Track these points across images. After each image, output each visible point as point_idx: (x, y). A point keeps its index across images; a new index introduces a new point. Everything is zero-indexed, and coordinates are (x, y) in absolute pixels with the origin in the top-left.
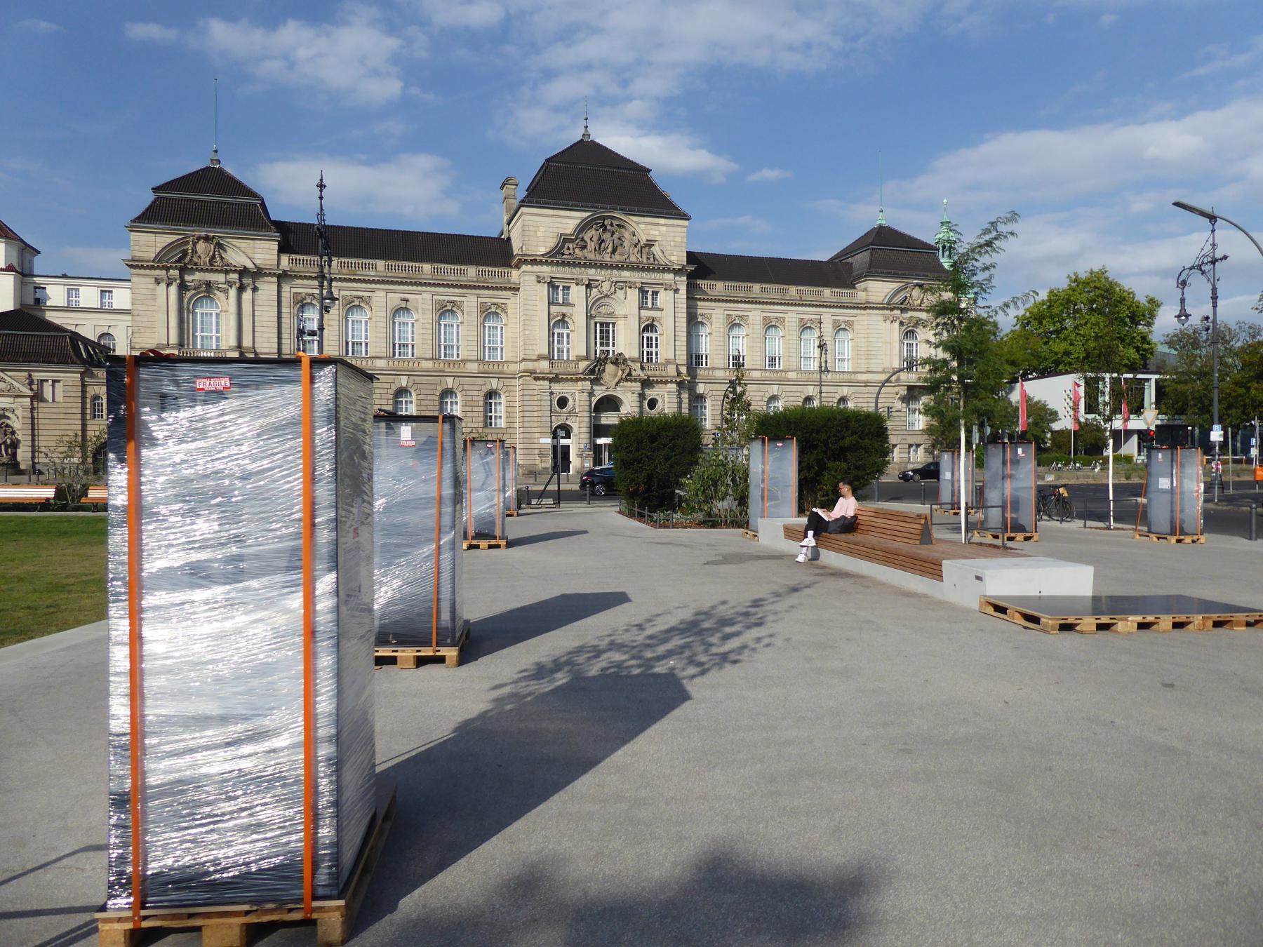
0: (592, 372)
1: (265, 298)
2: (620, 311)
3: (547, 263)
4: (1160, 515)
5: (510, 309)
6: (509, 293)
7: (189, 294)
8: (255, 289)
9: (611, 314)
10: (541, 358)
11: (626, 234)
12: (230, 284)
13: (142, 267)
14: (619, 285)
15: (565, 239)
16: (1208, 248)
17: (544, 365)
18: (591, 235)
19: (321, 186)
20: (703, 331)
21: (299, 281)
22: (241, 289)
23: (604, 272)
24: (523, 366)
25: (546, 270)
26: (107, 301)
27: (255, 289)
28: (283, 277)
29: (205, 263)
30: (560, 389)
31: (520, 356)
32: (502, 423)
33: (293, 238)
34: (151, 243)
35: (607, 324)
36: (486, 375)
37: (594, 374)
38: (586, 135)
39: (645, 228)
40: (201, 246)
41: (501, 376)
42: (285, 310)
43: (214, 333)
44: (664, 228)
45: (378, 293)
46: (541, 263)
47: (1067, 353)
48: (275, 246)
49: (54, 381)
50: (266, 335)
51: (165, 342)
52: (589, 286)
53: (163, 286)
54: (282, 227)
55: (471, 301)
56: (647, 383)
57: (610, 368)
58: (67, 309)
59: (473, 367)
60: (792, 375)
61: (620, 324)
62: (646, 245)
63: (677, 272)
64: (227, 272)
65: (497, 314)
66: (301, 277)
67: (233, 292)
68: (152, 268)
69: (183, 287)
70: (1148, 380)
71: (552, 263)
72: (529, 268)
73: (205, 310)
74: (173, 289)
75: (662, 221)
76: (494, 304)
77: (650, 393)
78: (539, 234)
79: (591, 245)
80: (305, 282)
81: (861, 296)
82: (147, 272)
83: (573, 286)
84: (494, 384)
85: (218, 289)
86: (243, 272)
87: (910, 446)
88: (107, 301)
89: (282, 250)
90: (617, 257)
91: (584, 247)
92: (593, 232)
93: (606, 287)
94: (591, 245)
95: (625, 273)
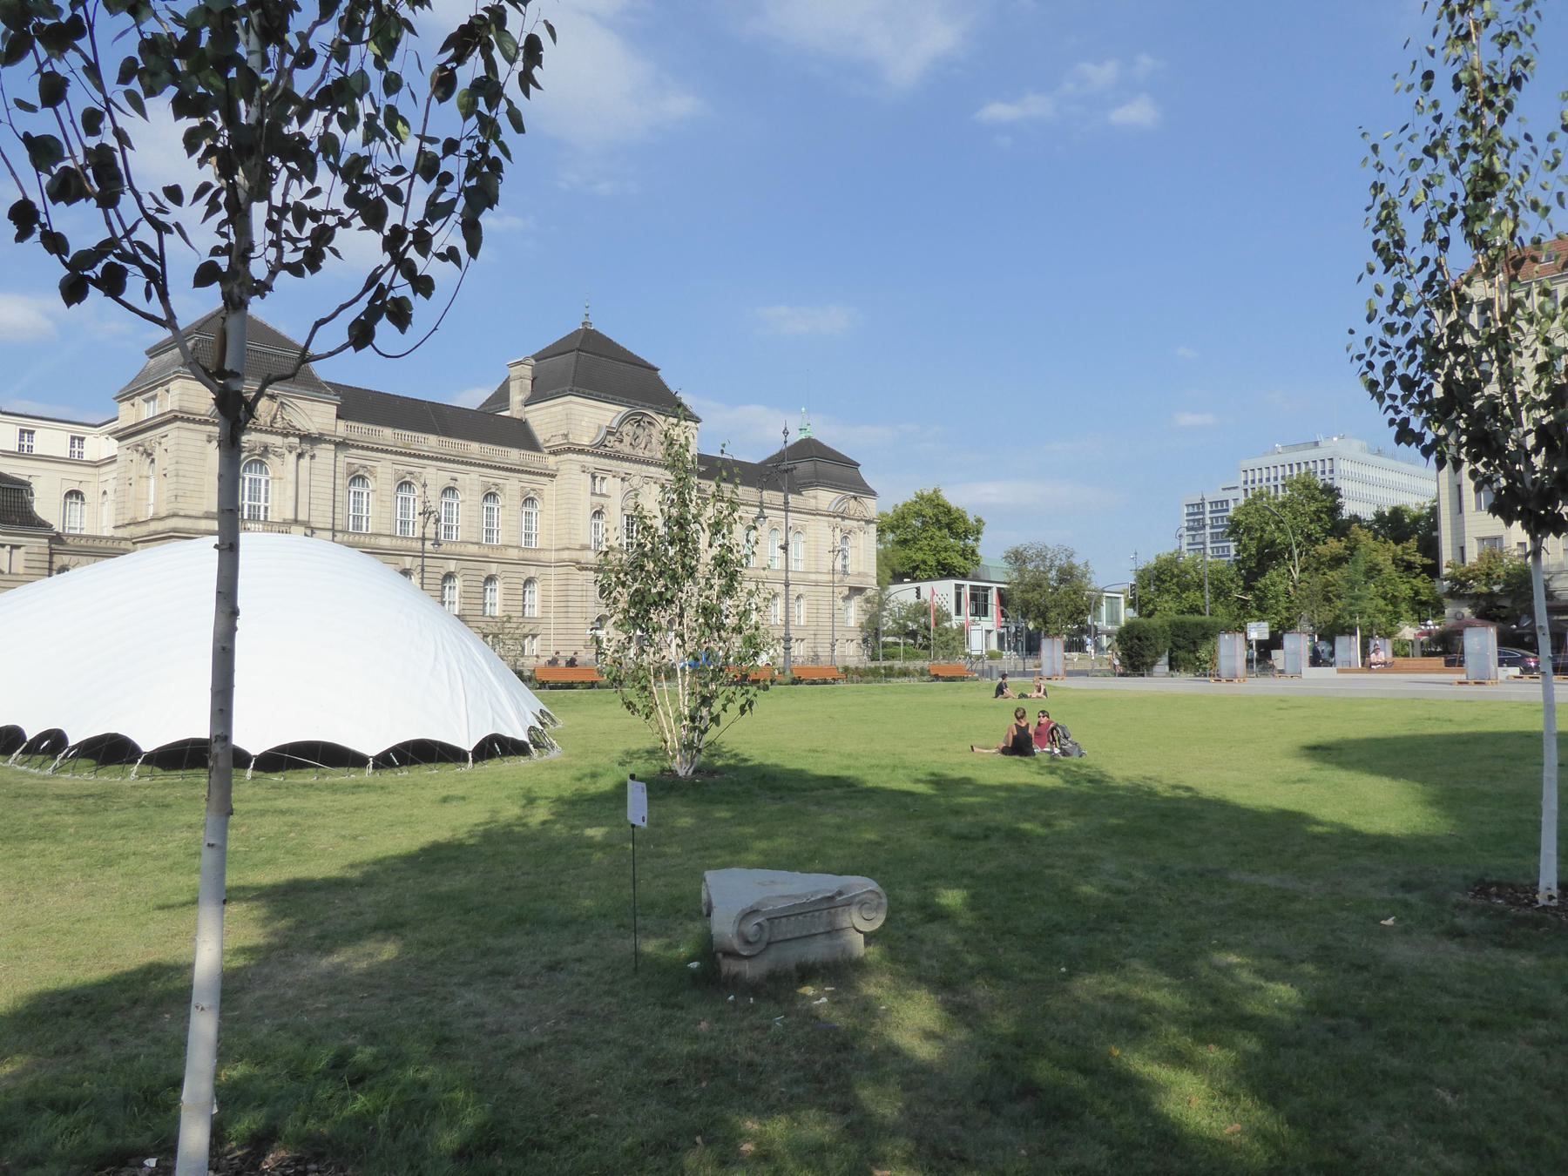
3: (592, 454)
4: (1224, 672)
8: (313, 457)
10: (585, 548)
12: (291, 449)
13: (194, 421)
18: (627, 428)
21: (354, 451)
22: (300, 456)
24: (566, 555)
26: (26, 443)
27: (313, 457)
28: (342, 445)
32: (536, 612)
36: (525, 562)
45: (429, 470)
46: (588, 453)
48: (334, 409)
49: (13, 547)
54: (338, 389)
55: (512, 486)
59: (513, 554)
64: (286, 435)
66: (357, 447)
67: (292, 458)
72: (574, 457)
73: (253, 476)
80: (360, 452)
81: (812, 504)
82: (197, 427)
83: (609, 477)
84: (532, 572)
86: (306, 438)
87: (526, 636)
88: (76, 449)
89: (338, 417)
93: (636, 481)
94: (627, 440)
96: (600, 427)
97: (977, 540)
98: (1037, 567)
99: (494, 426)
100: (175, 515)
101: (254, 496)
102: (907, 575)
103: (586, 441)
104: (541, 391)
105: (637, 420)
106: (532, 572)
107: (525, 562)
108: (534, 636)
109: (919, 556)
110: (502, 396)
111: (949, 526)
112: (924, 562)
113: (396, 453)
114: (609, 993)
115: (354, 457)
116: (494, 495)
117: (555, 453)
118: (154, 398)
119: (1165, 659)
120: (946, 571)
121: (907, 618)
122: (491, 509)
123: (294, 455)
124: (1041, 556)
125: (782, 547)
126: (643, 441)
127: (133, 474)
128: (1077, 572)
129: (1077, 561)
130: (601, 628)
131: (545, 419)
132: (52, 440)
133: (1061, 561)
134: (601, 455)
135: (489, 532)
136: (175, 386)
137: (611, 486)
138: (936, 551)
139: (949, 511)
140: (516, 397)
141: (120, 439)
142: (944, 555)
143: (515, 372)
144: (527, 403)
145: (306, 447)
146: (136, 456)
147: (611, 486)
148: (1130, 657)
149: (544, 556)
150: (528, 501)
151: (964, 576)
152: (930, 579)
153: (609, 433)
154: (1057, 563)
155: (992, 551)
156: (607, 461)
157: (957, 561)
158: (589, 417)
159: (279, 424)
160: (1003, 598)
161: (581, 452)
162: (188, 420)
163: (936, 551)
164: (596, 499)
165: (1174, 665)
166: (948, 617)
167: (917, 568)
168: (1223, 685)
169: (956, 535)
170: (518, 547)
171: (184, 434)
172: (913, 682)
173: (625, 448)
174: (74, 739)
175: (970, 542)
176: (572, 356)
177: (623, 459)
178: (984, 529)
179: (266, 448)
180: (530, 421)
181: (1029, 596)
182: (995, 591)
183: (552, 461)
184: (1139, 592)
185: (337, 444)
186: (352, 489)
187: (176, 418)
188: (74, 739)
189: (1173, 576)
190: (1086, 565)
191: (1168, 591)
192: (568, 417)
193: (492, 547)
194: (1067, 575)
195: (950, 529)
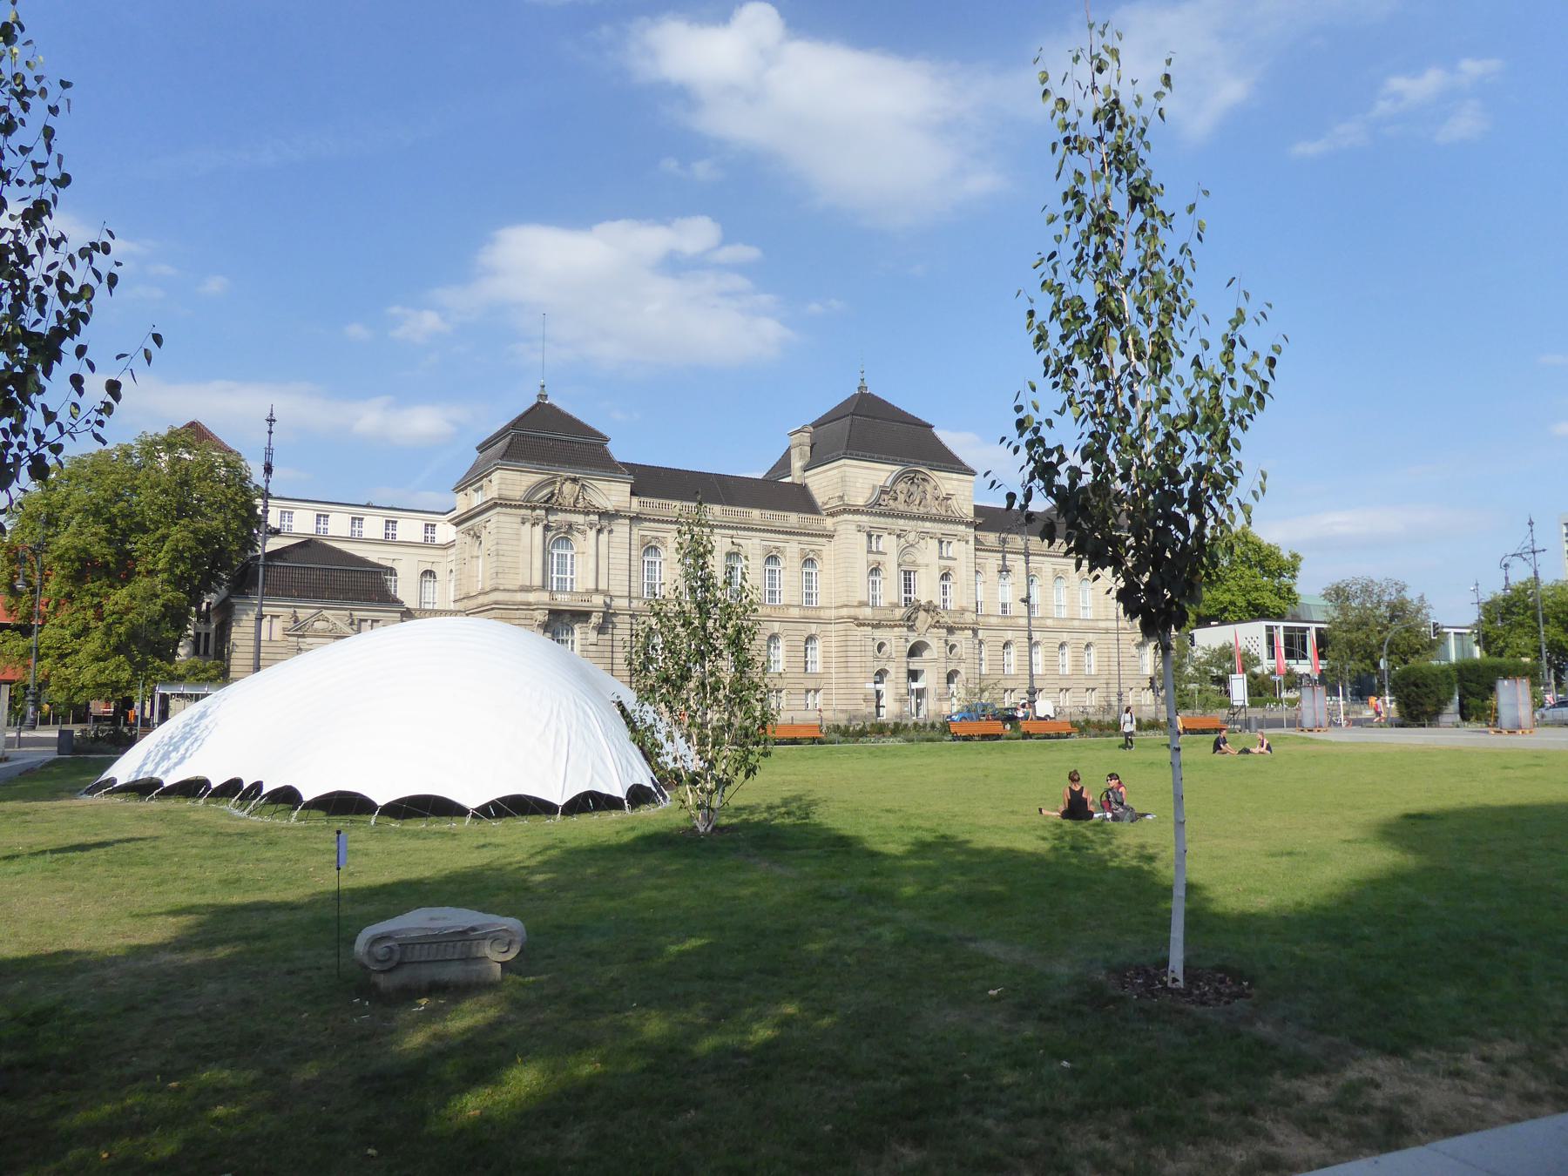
0: (909, 618)
3: (867, 513)
5: (824, 555)
7: (550, 534)
8: (611, 532)
9: (913, 563)
10: (862, 604)
11: (929, 488)
12: (591, 526)
14: (924, 535)
16: (1528, 542)
17: (866, 612)
18: (902, 486)
19: (271, 421)
20: (1037, 582)
21: (647, 524)
22: (599, 531)
23: (912, 523)
24: (844, 612)
25: (864, 520)
28: (636, 519)
30: (881, 634)
33: (648, 481)
34: (513, 481)
36: (806, 620)
37: (909, 622)
39: (947, 482)
40: (568, 487)
41: (820, 621)
46: (863, 513)
47: (1232, 603)
48: (628, 488)
51: (592, 586)
52: (899, 536)
53: (528, 525)
54: (632, 468)
55: (792, 549)
56: (951, 630)
57: (922, 614)
58: (349, 540)
59: (795, 612)
60: (1049, 622)
61: (922, 571)
63: (968, 524)
64: (587, 513)
65: (656, 548)
66: (650, 520)
67: (592, 534)
68: (520, 507)
69: (547, 528)
70: (1305, 630)
71: (871, 514)
74: (539, 529)
77: (952, 639)
79: (901, 497)
82: (514, 511)
83: (885, 535)
84: (813, 629)
85: (578, 530)
86: (604, 514)
87: (808, 691)
89: (633, 493)
93: (911, 537)
94: (901, 497)
95: (928, 524)
96: (874, 487)
97: (1293, 577)
98: (1363, 604)
99: (779, 494)
100: (496, 589)
101: (561, 570)
102: (1215, 618)
103: (860, 501)
104: (818, 458)
105: (911, 478)
108: (817, 691)
109: (1227, 597)
110: (784, 464)
111: (1260, 564)
112: (1232, 603)
115: (647, 530)
116: (775, 557)
117: (832, 515)
118: (481, 488)
119: (1453, 706)
120: (1257, 612)
121: (1208, 663)
123: (594, 532)
124: (1366, 590)
127: (466, 556)
128: (1411, 608)
129: (1411, 595)
130: (881, 682)
131: (823, 483)
132: (411, 528)
133: (1390, 596)
134: (876, 514)
135: (772, 593)
136: (496, 476)
138: (1244, 591)
139: (1258, 548)
140: (797, 464)
141: (457, 525)
142: (1255, 595)
143: (796, 439)
145: (604, 523)
146: (468, 539)
147: (888, 543)
148: (1407, 706)
149: (824, 614)
150: (808, 562)
151: (1280, 617)
152: (1240, 621)
153: (883, 492)
154: (1386, 598)
155: (1310, 587)
156: (882, 519)
157: (1269, 600)
158: (862, 478)
159: (581, 504)
160: (1323, 640)
161: (856, 512)
162: (506, 506)
163: (1244, 591)
164: (872, 557)
165: (1465, 714)
166: (1256, 661)
167: (1225, 609)
168: (1505, 737)
169: (1270, 574)
171: (502, 518)
172: (892, 742)
173: (900, 506)
174: (307, 796)
175: (1285, 580)
176: (847, 421)
177: (898, 517)
178: (1301, 565)
179: (570, 526)
181: (1353, 636)
182: (1313, 632)
183: (829, 523)
184: (1488, 627)
185: (631, 519)
187: (496, 505)
188: (307, 796)
189: (1527, 607)
190: (1422, 598)
191: (1521, 625)
192: (843, 479)
194: (1398, 611)
195: (1262, 567)
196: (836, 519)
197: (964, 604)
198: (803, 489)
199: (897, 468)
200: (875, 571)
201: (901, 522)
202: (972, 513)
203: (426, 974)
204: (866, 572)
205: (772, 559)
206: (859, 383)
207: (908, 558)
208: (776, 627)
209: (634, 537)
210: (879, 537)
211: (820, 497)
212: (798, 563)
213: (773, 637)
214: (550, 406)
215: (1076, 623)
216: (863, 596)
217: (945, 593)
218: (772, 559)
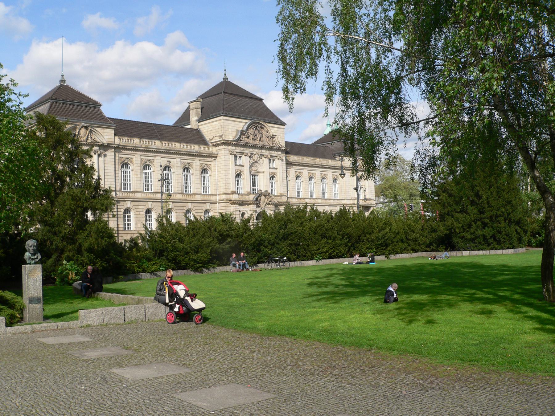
0: (256, 200)
1: (109, 160)
2: (260, 170)
5: (155, 163)
6: (212, 159)
8: (105, 155)
10: (233, 193)
14: (261, 156)
15: (243, 133)
17: (235, 197)
24: (224, 197)
28: (118, 148)
29: (84, 141)
31: (222, 191)
33: (124, 128)
35: (255, 176)
36: (204, 202)
38: (225, 79)
39: (273, 129)
40: (83, 131)
42: (117, 166)
43: (129, 181)
44: (276, 129)
45: (157, 158)
48: (113, 131)
50: (109, 180)
52: (250, 157)
55: (196, 163)
57: (263, 197)
59: (198, 198)
61: (261, 175)
62: (271, 137)
75: (276, 126)
76: (149, 160)
78: (230, 130)
83: (243, 156)
90: (261, 143)
91: (248, 138)
92: (252, 130)
93: (256, 157)
94: (251, 137)
95: (264, 151)
96: (237, 131)
103: (231, 138)
104: (205, 115)
106: (208, 206)
107: (145, 201)
113: (142, 151)
114: (305, 411)
115: (124, 155)
117: (216, 146)
122: (126, 172)
125: (355, 189)
126: (259, 136)
137: (244, 161)
140: (194, 118)
143: (193, 106)
144: (199, 121)
149: (213, 198)
150: (204, 170)
164: (237, 168)
170: (201, 194)
173: (251, 141)
176: (221, 96)
180: (201, 130)
183: (214, 150)
185: (115, 148)
186: (123, 170)
193: (188, 195)
196: (218, 148)
197: (282, 192)
198: (198, 131)
199: (249, 122)
200: (238, 175)
201: (251, 150)
202: (284, 145)
203: (314, 298)
204: (269, 177)
205: (186, 169)
206: (223, 76)
207: (254, 169)
208: (128, 205)
209: (117, 158)
210: (240, 157)
211: (207, 137)
212: (199, 171)
213: (127, 211)
214: (67, 86)
215: (332, 201)
216: (233, 188)
217: (272, 186)
218: (186, 169)
